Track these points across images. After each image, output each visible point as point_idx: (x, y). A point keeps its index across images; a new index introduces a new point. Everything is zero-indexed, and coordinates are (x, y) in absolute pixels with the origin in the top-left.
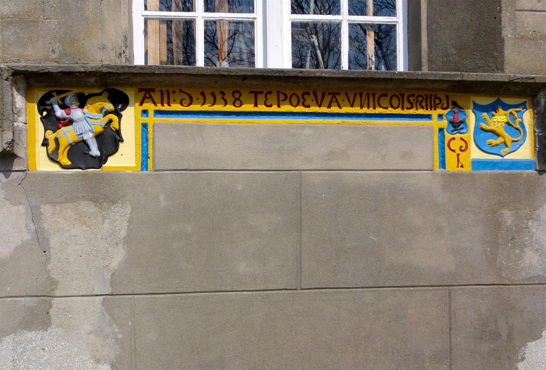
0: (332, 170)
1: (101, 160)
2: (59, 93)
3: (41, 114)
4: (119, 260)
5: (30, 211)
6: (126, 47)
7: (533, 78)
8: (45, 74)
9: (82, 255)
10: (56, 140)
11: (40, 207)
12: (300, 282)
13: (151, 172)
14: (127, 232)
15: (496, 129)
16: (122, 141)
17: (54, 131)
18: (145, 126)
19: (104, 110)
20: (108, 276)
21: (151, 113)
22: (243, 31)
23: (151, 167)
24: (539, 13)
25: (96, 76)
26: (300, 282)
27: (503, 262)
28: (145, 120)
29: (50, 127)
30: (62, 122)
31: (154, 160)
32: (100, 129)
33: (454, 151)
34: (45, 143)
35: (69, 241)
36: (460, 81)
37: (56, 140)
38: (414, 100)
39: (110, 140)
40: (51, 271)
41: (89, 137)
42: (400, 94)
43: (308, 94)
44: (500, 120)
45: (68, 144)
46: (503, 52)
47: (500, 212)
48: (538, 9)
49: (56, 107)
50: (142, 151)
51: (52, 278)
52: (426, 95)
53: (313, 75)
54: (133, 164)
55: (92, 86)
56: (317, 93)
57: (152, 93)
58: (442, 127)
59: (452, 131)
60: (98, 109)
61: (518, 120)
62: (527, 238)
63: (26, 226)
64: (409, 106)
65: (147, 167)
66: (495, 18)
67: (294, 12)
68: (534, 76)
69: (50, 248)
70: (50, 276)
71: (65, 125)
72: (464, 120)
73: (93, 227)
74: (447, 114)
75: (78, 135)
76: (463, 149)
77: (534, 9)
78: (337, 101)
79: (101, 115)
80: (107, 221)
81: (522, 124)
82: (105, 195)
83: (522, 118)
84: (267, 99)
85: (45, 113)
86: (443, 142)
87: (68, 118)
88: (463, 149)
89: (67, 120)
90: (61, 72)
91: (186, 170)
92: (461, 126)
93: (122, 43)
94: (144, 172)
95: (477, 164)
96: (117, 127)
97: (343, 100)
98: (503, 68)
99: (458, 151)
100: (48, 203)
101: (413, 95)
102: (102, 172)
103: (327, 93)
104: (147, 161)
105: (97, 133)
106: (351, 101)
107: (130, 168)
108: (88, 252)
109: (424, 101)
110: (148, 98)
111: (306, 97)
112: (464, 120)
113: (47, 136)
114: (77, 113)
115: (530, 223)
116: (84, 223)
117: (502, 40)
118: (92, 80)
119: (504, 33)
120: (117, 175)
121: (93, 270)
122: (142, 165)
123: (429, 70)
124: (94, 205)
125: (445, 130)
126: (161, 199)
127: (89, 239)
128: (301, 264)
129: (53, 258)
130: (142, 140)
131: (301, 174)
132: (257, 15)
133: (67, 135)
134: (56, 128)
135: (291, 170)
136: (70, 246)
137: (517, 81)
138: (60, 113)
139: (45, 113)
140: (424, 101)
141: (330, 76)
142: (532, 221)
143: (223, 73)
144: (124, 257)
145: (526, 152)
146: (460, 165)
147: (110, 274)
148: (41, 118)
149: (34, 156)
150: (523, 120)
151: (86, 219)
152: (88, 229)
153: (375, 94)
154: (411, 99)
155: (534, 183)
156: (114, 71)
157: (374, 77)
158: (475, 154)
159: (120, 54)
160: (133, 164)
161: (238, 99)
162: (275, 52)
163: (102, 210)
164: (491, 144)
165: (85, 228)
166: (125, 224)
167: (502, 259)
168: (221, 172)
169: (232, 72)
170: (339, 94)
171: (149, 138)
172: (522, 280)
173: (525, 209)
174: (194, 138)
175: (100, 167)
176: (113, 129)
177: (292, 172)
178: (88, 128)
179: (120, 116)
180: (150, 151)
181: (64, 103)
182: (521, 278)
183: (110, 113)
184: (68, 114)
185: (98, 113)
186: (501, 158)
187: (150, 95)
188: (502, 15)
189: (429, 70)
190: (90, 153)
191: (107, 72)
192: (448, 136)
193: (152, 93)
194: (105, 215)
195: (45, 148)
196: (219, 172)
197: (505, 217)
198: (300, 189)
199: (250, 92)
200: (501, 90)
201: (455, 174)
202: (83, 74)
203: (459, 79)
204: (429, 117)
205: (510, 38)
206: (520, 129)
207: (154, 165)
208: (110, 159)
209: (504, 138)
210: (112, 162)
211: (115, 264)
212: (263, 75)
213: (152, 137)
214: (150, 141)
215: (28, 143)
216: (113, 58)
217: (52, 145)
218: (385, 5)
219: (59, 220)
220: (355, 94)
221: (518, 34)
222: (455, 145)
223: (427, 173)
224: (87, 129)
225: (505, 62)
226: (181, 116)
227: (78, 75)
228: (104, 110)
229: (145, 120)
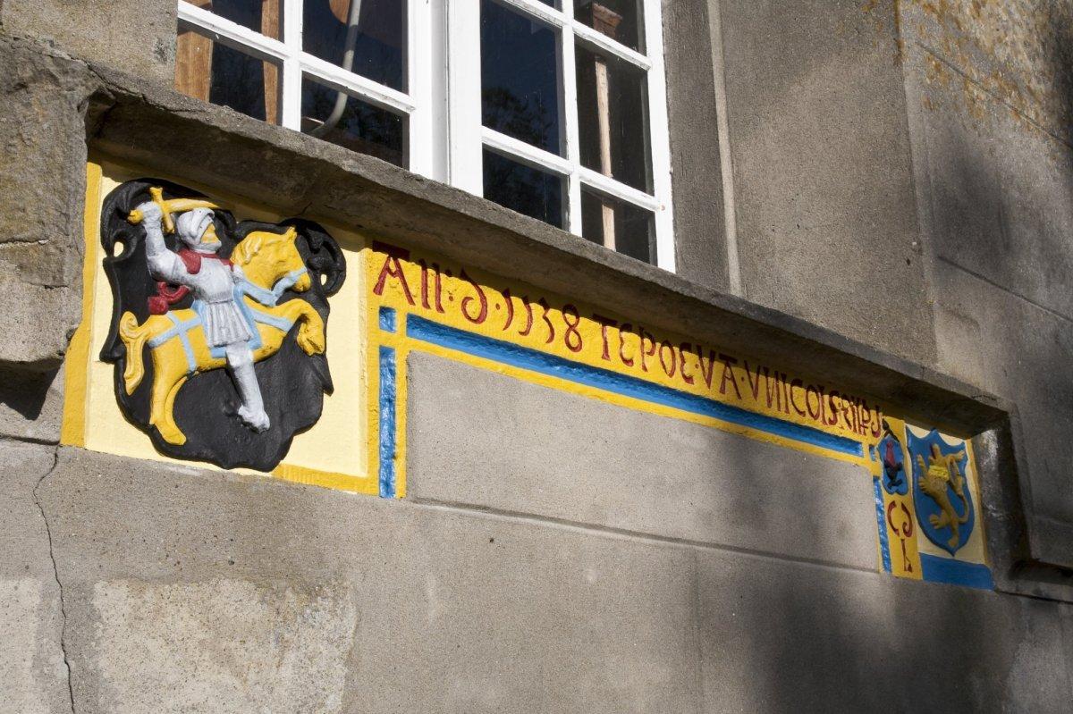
1: (264, 450)
2: (172, 192)
3: (109, 250)
5: (55, 602)
10: (148, 350)
11: (92, 592)
13: (404, 504)
18: (385, 352)
19: (285, 283)
21: (400, 321)
31: (410, 468)
37: (148, 350)
39: (298, 381)
41: (242, 359)
42: (819, 386)
45: (184, 371)
49: (156, 238)
56: (703, 348)
57: (402, 262)
63: (39, 661)
71: (175, 306)
73: (252, 676)
75: (218, 346)
80: (291, 657)
82: (289, 560)
87: (187, 284)
100: (121, 576)
116: (225, 659)
120: (305, 501)
123: (217, 97)
124: (257, 597)
126: (431, 592)
133: (178, 341)
151: (232, 645)
152: (239, 687)
165: (227, 678)
166: (340, 670)
174: (497, 414)
178: (244, 330)
179: (323, 308)
186: (949, 556)
187: (398, 265)
189: (217, 97)
190: (242, 411)
195: (111, 367)
207: (411, 484)
210: (307, 454)
212: (656, 284)
214: (400, 407)
219: (151, 644)
224: (241, 333)
229: (386, 338)
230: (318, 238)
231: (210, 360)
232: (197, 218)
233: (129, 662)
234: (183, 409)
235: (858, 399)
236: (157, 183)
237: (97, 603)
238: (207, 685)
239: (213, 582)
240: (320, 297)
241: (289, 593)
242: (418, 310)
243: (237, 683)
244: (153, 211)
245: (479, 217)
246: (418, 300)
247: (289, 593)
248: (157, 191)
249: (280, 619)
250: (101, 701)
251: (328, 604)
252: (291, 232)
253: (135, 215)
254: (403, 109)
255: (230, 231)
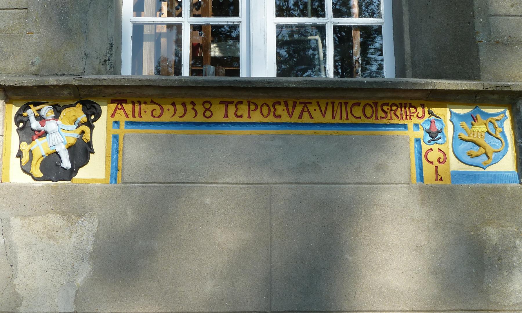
0: (303, 183)
1: (70, 174)
2: (36, 104)
3: (18, 126)
4: (84, 276)
6: (111, 54)
7: (509, 86)
8: (21, 87)
9: (47, 270)
10: (30, 152)
12: (271, 304)
14: (93, 247)
15: (475, 139)
16: (93, 153)
17: (29, 143)
18: (116, 137)
20: (72, 293)
21: (122, 124)
22: (227, 36)
23: (120, 180)
24: (513, 18)
25: (69, 89)
26: (271, 304)
27: (490, 285)
28: (116, 131)
29: (25, 139)
30: (37, 133)
32: (72, 141)
33: (432, 163)
34: (20, 155)
35: (36, 256)
36: (431, 91)
37: (30, 152)
38: (388, 109)
39: (81, 152)
40: (17, 286)
43: (279, 103)
44: (480, 130)
45: (41, 156)
46: (479, 59)
47: (484, 229)
48: (512, 14)
49: (32, 119)
50: (112, 163)
51: (18, 294)
52: (401, 104)
53: (281, 86)
54: (103, 177)
55: (67, 99)
57: (124, 105)
58: (418, 137)
59: (429, 142)
60: (71, 120)
61: (499, 129)
62: (515, 259)
64: (383, 115)
65: (116, 179)
66: (469, 23)
67: (278, 16)
68: (509, 83)
69: (17, 263)
70: (15, 291)
71: (40, 137)
72: (441, 129)
73: (60, 241)
74: (424, 123)
76: (441, 160)
77: (508, 14)
78: (308, 111)
79: (75, 127)
80: (74, 235)
81: (503, 133)
83: (502, 127)
84: (237, 109)
85: (21, 125)
86: (420, 153)
88: (441, 160)
89: (41, 133)
90: (35, 86)
91: (155, 183)
92: (439, 135)
93: (108, 51)
94: (113, 184)
95: (457, 176)
96: (89, 139)
97: (315, 110)
98: (480, 75)
99: (436, 163)
100: (18, 216)
101: (387, 104)
102: (72, 184)
103: (298, 103)
104: (116, 174)
105: (70, 145)
106: (323, 110)
107: (99, 181)
108: (54, 268)
109: (399, 109)
110: (120, 109)
111: (277, 107)
112: (441, 129)
113: (22, 148)
114: (51, 125)
115: (518, 242)
117: (477, 47)
118: (66, 92)
119: (478, 38)
121: (58, 286)
122: (111, 177)
125: (422, 141)
126: (129, 213)
127: (56, 253)
128: (271, 284)
129: (19, 272)
130: (112, 151)
131: (271, 187)
132: (241, 20)
133: (41, 148)
134: (31, 139)
135: (260, 184)
136: (37, 261)
137: (492, 89)
138: (35, 125)
139: (21, 125)
140: (399, 109)
141: (298, 86)
142: (519, 239)
143: (190, 85)
144: (90, 273)
145: (507, 164)
146: (439, 178)
147: (74, 291)
148: (17, 130)
149: (8, 167)
150: (503, 129)
153: (347, 103)
154: (385, 108)
155: (519, 198)
156: (85, 84)
157: (342, 87)
158: (454, 165)
159: (105, 62)
160: (103, 177)
161: (208, 109)
162: (260, 60)
163: (70, 224)
164: (472, 155)
165: (52, 242)
167: (489, 282)
168: (189, 185)
169: (200, 83)
170: (310, 103)
171: (119, 149)
172: (512, 305)
173: (512, 226)
175: (70, 179)
176: (85, 140)
177: (262, 185)
179: (92, 127)
180: (120, 164)
181: (39, 114)
182: (511, 303)
183: (83, 124)
184: (42, 126)
185: (71, 124)
186: (482, 170)
188: (475, 20)
191: (79, 85)
192: (425, 147)
193: (124, 105)
194: (72, 229)
196: (187, 185)
197: (490, 235)
198: (271, 203)
199: (221, 103)
200: (477, 98)
201: (434, 187)
202: (57, 87)
203: (430, 88)
204: (405, 126)
205: (484, 44)
206: (501, 139)
207: (123, 178)
208: (80, 170)
209: (485, 149)
210: (83, 174)
211: (80, 280)
212: (231, 87)
213: (122, 148)
215: (4, 155)
216: (97, 66)
217: (26, 157)
218: (368, 8)
219: (27, 233)
220: (327, 103)
221: (493, 39)
222: (434, 156)
223: (404, 187)
225: (481, 69)
226: (239, 127)
227: (52, 88)
228: (77, 122)
229: (116, 131)
230: (88, 106)
231: (51, 150)
232: (47, 110)
233: (21, 238)
234: (43, 167)
235: (401, 104)
236: (31, 103)
237: (11, 223)
238: (45, 244)
239: (47, 215)
240: (90, 124)
241: (73, 217)
242: (131, 119)
243: (55, 243)
244: (31, 113)
245: (134, 85)
246: (130, 115)
247: (73, 217)
248: (31, 106)
249: (70, 224)
250: (13, 248)
251: (88, 219)
252: (79, 107)
253: (25, 114)
254: (237, 24)
255: (58, 112)
